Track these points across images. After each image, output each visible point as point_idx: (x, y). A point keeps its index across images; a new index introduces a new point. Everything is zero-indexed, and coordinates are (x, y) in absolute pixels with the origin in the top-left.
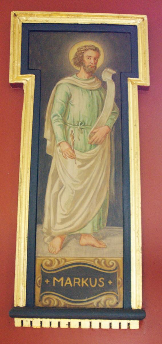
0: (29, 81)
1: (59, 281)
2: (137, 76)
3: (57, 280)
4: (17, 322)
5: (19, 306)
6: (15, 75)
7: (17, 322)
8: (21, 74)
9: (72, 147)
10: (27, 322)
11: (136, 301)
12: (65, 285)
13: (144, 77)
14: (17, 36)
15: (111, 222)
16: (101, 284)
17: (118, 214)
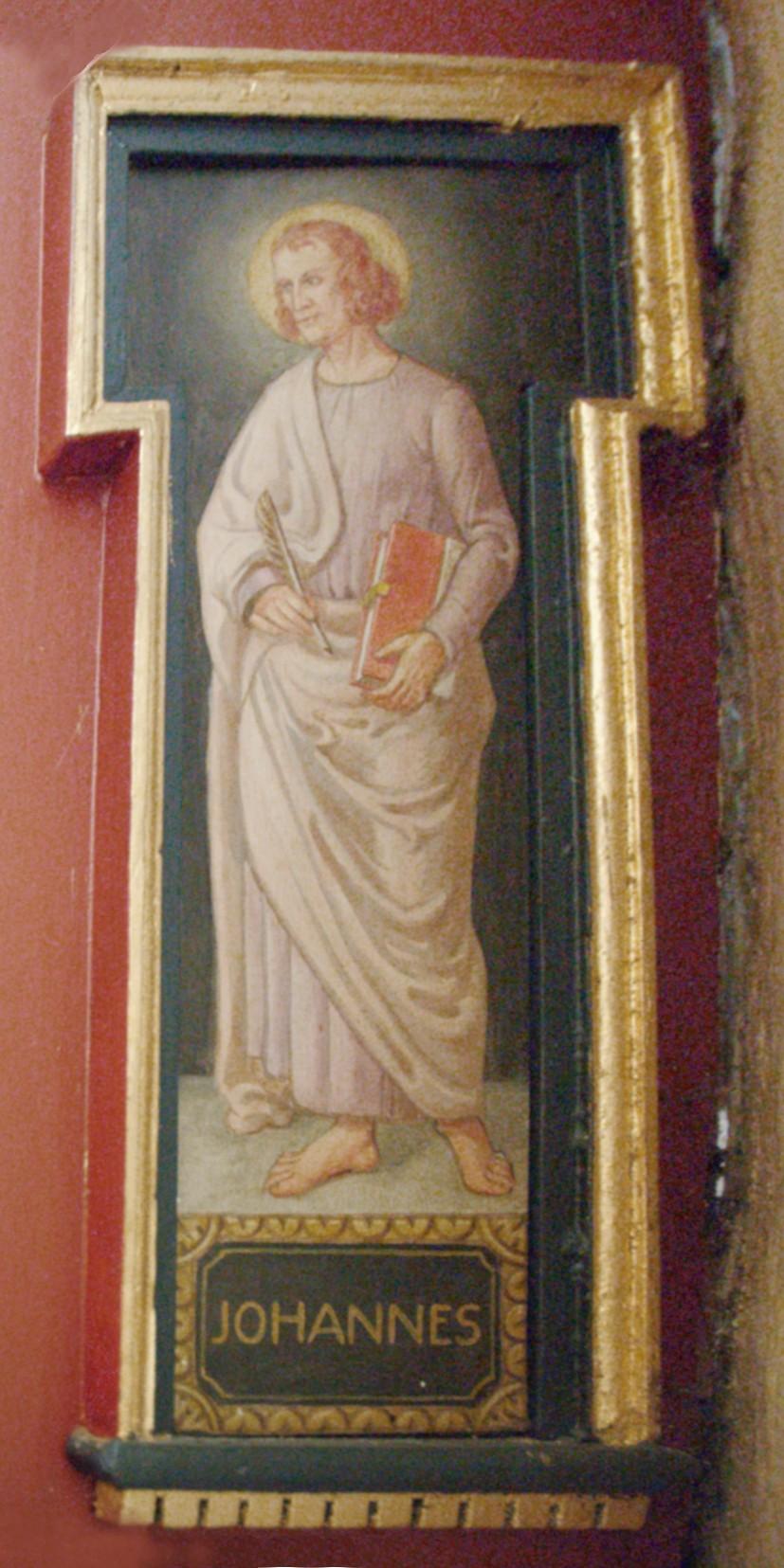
7: (136, 1505)
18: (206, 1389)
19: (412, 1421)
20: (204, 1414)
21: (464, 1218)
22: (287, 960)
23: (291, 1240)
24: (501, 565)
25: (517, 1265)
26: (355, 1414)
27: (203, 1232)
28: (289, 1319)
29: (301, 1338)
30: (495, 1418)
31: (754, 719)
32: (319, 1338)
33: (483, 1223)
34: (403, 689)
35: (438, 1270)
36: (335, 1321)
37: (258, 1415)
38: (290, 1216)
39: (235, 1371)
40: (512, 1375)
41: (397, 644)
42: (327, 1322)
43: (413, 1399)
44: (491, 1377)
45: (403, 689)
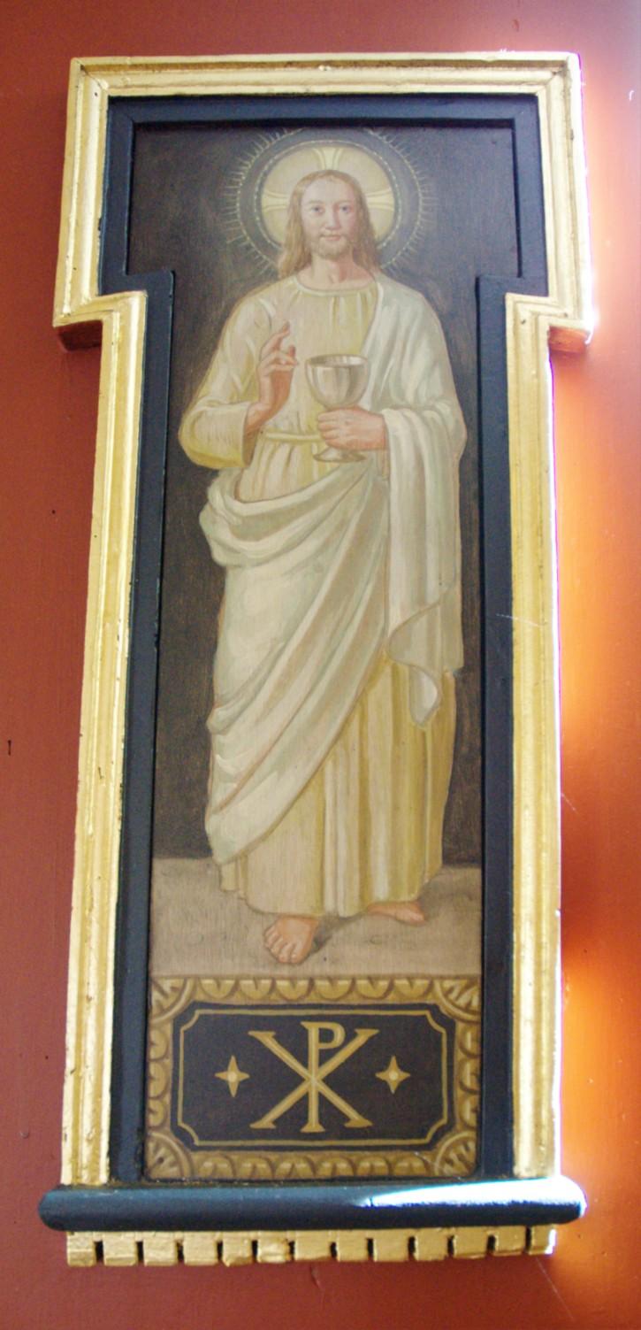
7: (79, 1245)
18: (180, 1134)
20: (176, 1162)
21: (424, 977)
22: (353, 708)
24: (302, 132)
25: (469, 1022)
26: (202, 1162)
30: (450, 1162)
31: (262, 272)
33: (437, 985)
37: (426, 1163)
38: (340, 978)
39: (217, 1119)
43: (249, 1143)
44: (444, 1121)
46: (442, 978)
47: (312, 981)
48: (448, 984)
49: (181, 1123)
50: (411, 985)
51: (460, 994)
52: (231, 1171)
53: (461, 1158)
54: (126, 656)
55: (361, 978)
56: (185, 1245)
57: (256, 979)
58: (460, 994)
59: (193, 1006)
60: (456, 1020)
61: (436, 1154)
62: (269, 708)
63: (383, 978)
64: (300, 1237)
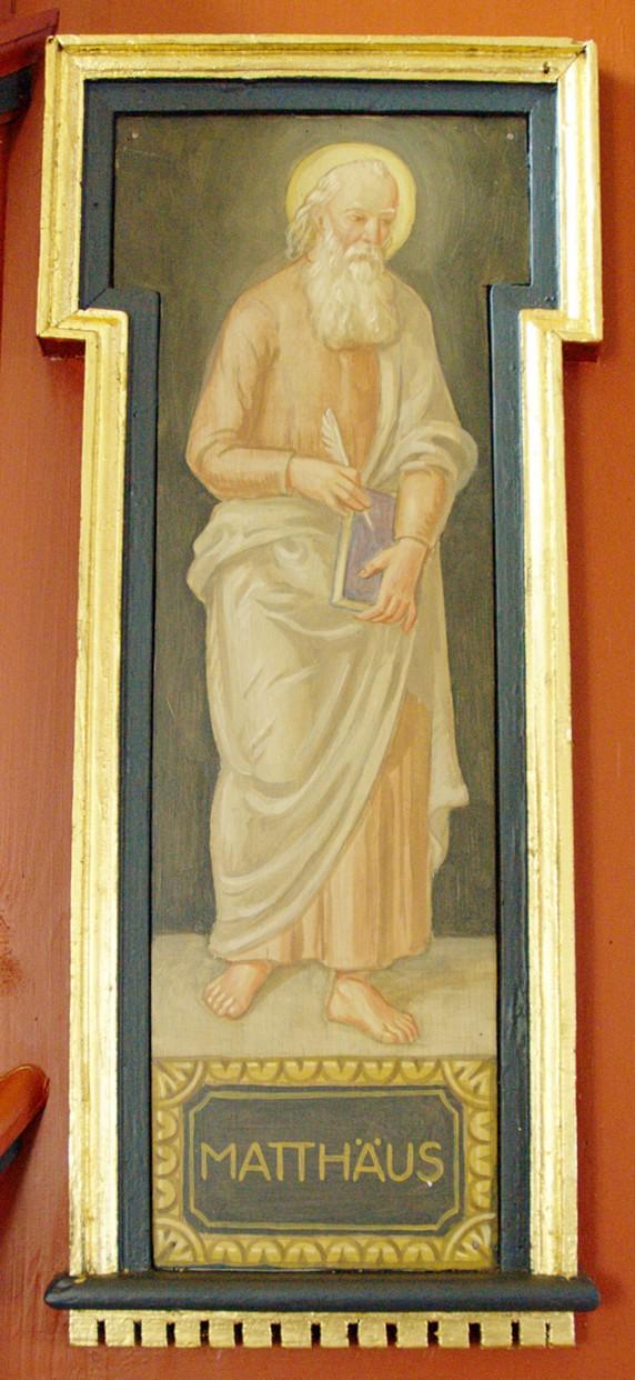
0: (106, 337)
1: (219, 1158)
2: (552, 303)
3: (213, 1153)
4: (82, 1328)
5: (98, 1273)
6: (57, 306)
7: (82, 1328)
8: (88, 82)
9: (27, 1267)
10: (119, 1326)
11: (553, 1248)
12: (355, 1178)
13: (580, 308)
14: (63, 133)
15: (448, 919)
16: (429, 1169)
17: (481, 889)
19: (302, 1254)
23: (234, 1082)
26: (213, 1246)
27: (190, 1076)
28: (335, 1158)
29: (233, 1175)
32: (249, 1174)
33: (446, 1065)
34: (393, 604)
35: (417, 1113)
36: (376, 1161)
37: (319, 1247)
38: (424, 1059)
39: (218, 1205)
40: (477, 1207)
41: (377, 562)
42: (255, 1161)
44: (455, 1211)
45: (393, 604)
46: (452, 1058)
47: (439, 1064)
48: (459, 1065)
49: (193, 1210)
50: (418, 1068)
51: (175, 1079)
52: (240, 1255)
53: (476, 1246)
54: (81, 663)
55: (290, 1059)
56: (522, 1327)
57: (300, 1061)
58: (175, 1079)
59: (204, 1090)
60: (463, 1105)
61: (448, 1240)
62: (357, 720)
63: (272, 1060)
64: (289, 1321)
